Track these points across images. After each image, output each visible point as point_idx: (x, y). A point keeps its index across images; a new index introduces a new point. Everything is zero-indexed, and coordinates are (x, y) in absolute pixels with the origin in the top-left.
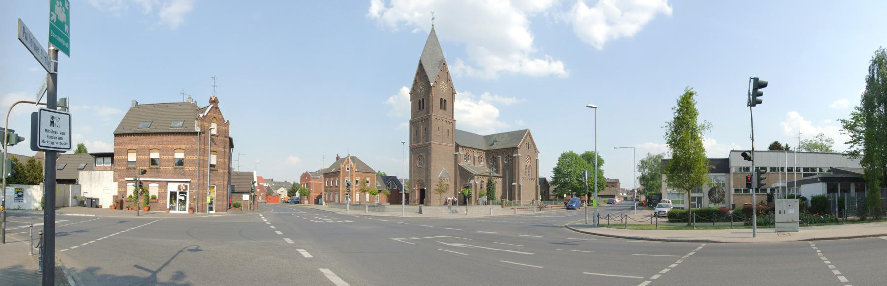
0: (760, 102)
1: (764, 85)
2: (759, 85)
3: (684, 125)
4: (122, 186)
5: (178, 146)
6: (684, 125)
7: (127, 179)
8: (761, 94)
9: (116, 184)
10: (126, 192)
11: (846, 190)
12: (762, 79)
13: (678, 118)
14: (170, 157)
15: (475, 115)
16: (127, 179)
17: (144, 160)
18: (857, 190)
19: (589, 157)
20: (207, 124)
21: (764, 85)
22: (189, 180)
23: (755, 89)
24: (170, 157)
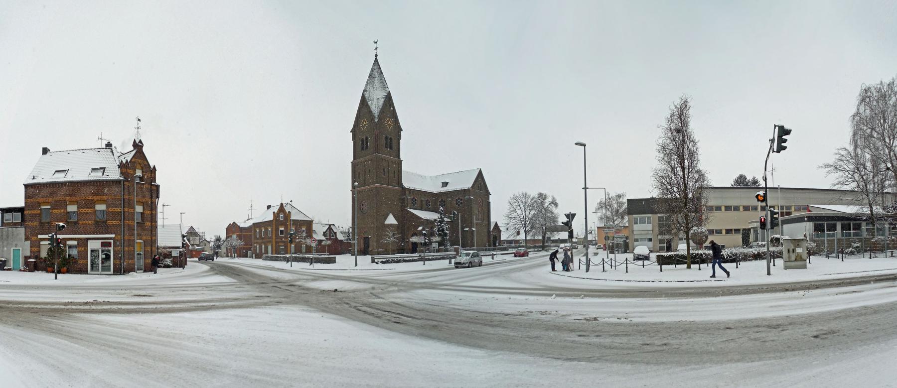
0: (785, 148)
1: (788, 132)
2: (783, 132)
3: (680, 145)
4: (36, 244)
5: (99, 197)
6: (680, 145)
7: (40, 236)
8: (785, 141)
9: (29, 242)
10: (39, 251)
11: (832, 228)
12: (787, 127)
13: (50, 249)
14: (90, 210)
15: (425, 165)
16: (40, 236)
17: (59, 214)
18: (843, 228)
19: (865, 97)
20: (130, 171)
21: (788, 132)
22: (113, 236)
23: (780, 137)
24: (90, 210)
